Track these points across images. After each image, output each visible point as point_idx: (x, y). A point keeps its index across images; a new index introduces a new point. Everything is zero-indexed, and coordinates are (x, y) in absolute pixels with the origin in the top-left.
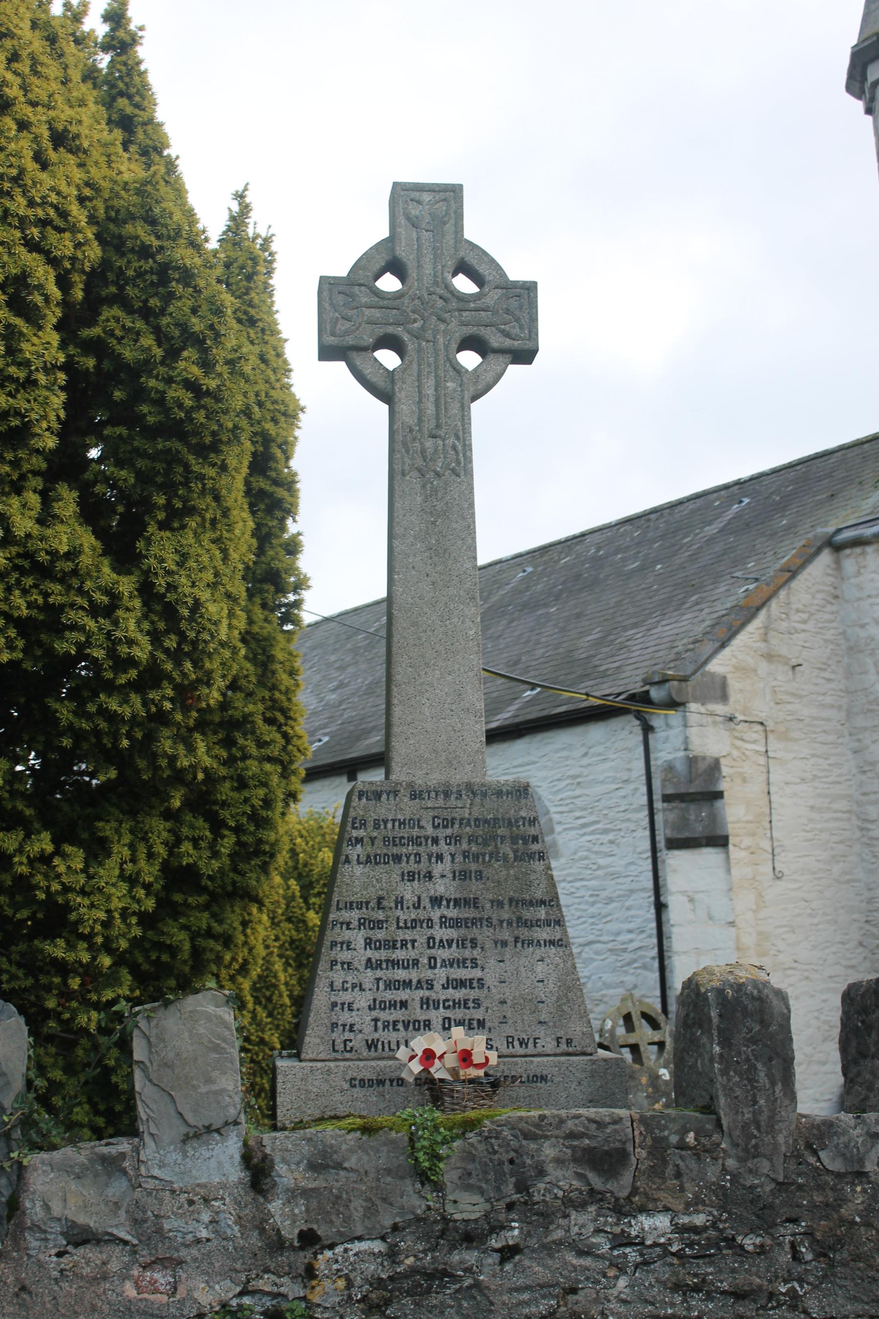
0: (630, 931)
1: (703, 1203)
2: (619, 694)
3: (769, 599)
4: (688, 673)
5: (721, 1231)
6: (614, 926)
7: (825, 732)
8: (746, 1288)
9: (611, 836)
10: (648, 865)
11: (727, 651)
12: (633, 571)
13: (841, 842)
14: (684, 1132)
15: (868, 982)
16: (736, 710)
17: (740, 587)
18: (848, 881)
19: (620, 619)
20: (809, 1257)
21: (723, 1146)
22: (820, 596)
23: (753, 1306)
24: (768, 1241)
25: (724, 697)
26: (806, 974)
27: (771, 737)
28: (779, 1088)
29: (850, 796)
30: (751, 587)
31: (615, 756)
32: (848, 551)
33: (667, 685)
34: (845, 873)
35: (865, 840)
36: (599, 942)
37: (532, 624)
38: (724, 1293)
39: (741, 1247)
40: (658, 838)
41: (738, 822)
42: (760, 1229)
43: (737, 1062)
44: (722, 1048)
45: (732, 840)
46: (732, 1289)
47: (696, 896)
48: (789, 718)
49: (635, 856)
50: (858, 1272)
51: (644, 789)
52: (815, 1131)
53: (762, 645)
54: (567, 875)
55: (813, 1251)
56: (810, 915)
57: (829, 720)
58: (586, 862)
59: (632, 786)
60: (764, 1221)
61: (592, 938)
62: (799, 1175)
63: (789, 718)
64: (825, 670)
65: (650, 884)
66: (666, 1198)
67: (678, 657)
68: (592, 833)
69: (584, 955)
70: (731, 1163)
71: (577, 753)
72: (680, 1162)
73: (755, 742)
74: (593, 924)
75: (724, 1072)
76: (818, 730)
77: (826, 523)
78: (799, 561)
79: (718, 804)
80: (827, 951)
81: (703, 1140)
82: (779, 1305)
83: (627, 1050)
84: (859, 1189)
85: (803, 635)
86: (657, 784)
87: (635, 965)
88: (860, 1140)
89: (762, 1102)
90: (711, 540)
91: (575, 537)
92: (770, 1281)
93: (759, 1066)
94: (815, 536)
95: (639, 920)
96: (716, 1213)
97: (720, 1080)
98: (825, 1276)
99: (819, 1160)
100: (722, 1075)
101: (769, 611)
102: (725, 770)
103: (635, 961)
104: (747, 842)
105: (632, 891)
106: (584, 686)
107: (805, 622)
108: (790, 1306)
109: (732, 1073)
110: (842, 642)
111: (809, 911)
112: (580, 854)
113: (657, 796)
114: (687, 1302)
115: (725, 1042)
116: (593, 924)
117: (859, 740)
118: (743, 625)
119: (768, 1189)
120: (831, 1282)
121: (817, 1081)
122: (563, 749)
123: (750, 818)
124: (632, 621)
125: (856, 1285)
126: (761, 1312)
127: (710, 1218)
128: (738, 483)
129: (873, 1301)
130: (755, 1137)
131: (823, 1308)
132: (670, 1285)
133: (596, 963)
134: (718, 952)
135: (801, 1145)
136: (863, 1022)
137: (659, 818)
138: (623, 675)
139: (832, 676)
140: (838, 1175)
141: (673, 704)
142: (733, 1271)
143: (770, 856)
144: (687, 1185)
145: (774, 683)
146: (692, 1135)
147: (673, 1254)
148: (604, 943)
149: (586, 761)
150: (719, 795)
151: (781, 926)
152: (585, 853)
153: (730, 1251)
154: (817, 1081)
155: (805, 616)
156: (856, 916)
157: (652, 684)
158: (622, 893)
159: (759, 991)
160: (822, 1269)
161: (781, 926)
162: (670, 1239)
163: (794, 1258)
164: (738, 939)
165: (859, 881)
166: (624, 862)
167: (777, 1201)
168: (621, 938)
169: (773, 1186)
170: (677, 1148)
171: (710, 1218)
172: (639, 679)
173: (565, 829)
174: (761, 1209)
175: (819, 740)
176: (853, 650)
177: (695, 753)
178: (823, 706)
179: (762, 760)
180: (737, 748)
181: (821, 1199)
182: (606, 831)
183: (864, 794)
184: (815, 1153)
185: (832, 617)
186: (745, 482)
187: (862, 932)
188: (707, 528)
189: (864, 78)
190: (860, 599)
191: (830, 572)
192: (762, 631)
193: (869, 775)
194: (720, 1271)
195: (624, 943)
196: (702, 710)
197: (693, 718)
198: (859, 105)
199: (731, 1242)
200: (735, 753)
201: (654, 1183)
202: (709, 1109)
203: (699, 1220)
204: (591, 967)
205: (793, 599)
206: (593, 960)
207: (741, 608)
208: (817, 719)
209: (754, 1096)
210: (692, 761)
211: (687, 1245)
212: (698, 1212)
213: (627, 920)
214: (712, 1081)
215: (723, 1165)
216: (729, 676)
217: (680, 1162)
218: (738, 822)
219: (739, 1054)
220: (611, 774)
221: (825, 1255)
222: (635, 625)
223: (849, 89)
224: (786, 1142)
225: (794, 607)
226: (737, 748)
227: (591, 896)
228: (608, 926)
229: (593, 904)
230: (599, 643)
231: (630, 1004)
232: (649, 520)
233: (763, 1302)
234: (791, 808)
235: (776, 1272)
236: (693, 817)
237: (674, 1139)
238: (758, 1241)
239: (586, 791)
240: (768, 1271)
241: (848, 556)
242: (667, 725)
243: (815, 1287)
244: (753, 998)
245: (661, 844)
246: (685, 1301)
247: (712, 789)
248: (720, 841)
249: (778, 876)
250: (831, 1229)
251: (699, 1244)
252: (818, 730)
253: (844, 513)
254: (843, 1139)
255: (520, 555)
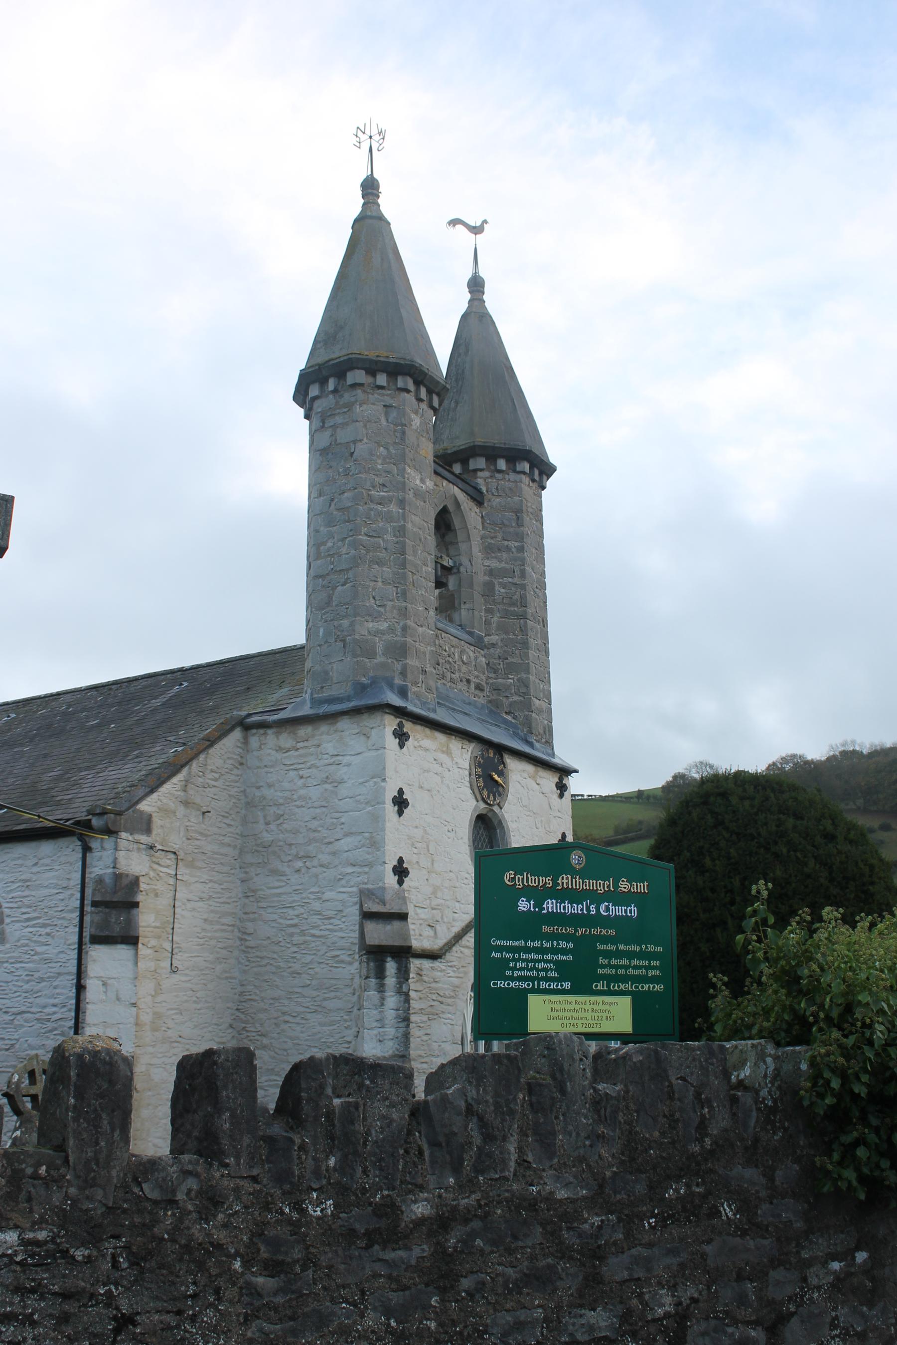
0: (54, 1005)
1: (47, 1222)
2: (68, 820)
3: (191, 760)
4: (123, 809)
5: (58, 1245)
6: (42, 1001)
7: (221, 863)
8: (73, 1290)
9: (48, 930)
10: (74, 955)
11: (155, 796)
12: (93, 726)
13: (224, 948)
14: (38, 1165)
15: (197, 1054)
16: (157, 841)
17: (172, 748)
18: (227, 978)
19: (77, 762)
20: (125, 1265)
21: (68, 1177)
22: (230, 762)
23: (76, 1304)
24: (95, 1253)
25: (148, 831)
26: (187, 1047)
27: (180, 864)
28: (117, 1133)
29: (235, 914)
30: (180, 749)
31: (58, 868)
32: (254, 731)
33: (106, 816)
34: (226, 972)
35: (243, 948)
36: (29, 1012)
37: (8, 758)
38: (53, 1294)
39: (73, 1257)
40: (84, 934)
41: (148, 926)
42: (89, 1243)
43: (87, 1112)
44: (76, 1100)
45: (141, 940)
46: (61, 1291)
47: (109, 982)
48: (196, 851)
49: (66, 947)
50: (161, 1277)
51: (78, 895)
52: (141, 1168)
53: (182, 794)
54: (9, 958)
55: (129, 1261)
56: (195, 1002)
57: (226, 855)
58: (25, 948)
59: (69, 892)
60: (93, 1235)
61: (23, 1008)
62: (125, 1201)
63: (196, 851)
64: (227, 817)
65: (74, 970)
66: (16, 1217)
67: (117, 796)
68: (34, 926)
69: (16, 1022)
70: (72, 1191)
71: (29, 863)
72: (32, 1189)
73: (168, 867)
74: (26, 997)
75: (76, 1119)
76: (216, 862)
77: (240, 710)
78: (217, 734)
79: (135, 911)
80: (205, 1030)
81: (52, 1172)
82: (97, 1304)
83: (29, 1099)
84: (169, 1213)
85: (213, 789)
86: (89, 891)
87: (55, 1032)
88: (175, 1176)
89: (103, 1144)
90: (155, 711)
91: (52, 695)
92: (92, 1285)
93: (104, 1116)
94: (232, 717)
95: (62, 997)
96: (55, 1230)
97: (72, 1125)
98: (136, 1281)
99: (142, 1190)
100: (74, 1122)
101: (190, 768)
102: (143, 886)
103: (56, 1029)
104: (153, 942)
105: (59, 974)
106: (42, 811)
107: (216, 780)
108: (105, 1304)
109: (81, 1120)
110: (243, 797)
111: (195, 999)
112: (22, 942)
113: (87, 902)
114: (24, 1302)
115: (79, 1096)
116: (26, 997)
117: (246, 873)
118: (174, 774)
119: (99, 1212)
120: (140, 1285)
121: (152, 1131)
122: (19, 858)
123: (158, 924)
124: (85, 765)
125: (159, 1287)
126: (82, 1309)
127: (51, 1234)
128: (181, 670)
129: (170, 1299)
130: (94, 1171)
131: (132, 1305)
132: (11, 1288)
133: (24, 1029)
134: (121, 1026)
135: (129, 1179)
136: (190, 1085)
137: (87, 919)
138: (74, 805)
139: (232, 823)
140: (155, 1202)
141: (110, 832)
142: (64, 1276)
143: (170, 955)
144: (35, 1208)
145: (187, 824)
146: (44, 1168)
147: (17, 1263)
148: (33, 1013)
149: (35, 869)
150: (136, 905)
151: (172, 1009)
152: (27, 942)
153: (63, 1261)
154: (152, 1131)
155: (217, 776)
156: (229, 1005)
157: (94, 815)
158: (52, 975)
159: (111, 1058)
160: (134, 1275)
161: (172, 1009)
162: (16, 1251)
163: (113, 1266)
164: (137, 1017)
165: (235, 978)
166: (56, 951)
167: (106, 1222)
168: (47, 1010)
169: (104, 1209)
170: (31, 1178)
171: (51, 1234)
172: (84, 809)
173: (13, 921)
174: (92, 1228)
175: (216, 869)
176: (250, 804)
177: (120, 871)
178: (223, 844)
179: (172, 881)
180: (154, 870)
181: (139, 1220)
182: (44, 926)
183: (246, 913)
184: (139, 1184)
185: (237, 778)
186: (187, 670)
187: (234, 1017)
188: (153, 701)
189: (307, 394)
190: (259, 767)
191: (240, 745)
192: (184, 783)
193: (251, 899)
194: (54, 1277)
195: (49, 1014)
196: (130, 838)
197: (122, 844)
198: (301, 411)
199: (65, 1253)
200: (152, 874)
201: (8, 1206)
202: (61, 1148)
203: (42, 1235)
204: (20, 1031)
205: (209, 761)
206: (22, 1026)
207: (170, 764)
208: (217, 853)
209: (97, 1139)
210: (118, 877)
211: (29, 1256)
212: (41, 1229)
213: (53, 996)
214: (65, 1126)
215: (66, 1192)
216: (154, 815)
217: (32, 1189)
218: (148, 926)
219: (89, 1105)
220: (55, 882)
221: (138, 1264)
222: (88, 768)
223: (295, 398)
224: (118, 1176)
225: (209, 768)
226: (154, 870)
227: (27, 975)
228: (38, 1000)
229: (28, 982)
230: (58, 779)
231: (35, 1063)
232: (110, 689)
233: (85, 1301)
234: (189, 920)
235: (98, 1277)
236: (113, 920)
237: (29, 1171)
238: (87, 1252)
239: (33, 893)
240: (92, 1276)
241: (254, 735)
242: (102, 847)
243: (128, 1289)
244: (104, 1062)
245: (86, 939)
246: (22, 1300)
247: (130, 900)
248: (132, 940)
249: (174, 970)
250: (144, 1244)
251: (39, 1255)
252: (216, 862)
253: (255, 703)
254: (162, 1174)
255: (7, 704)
